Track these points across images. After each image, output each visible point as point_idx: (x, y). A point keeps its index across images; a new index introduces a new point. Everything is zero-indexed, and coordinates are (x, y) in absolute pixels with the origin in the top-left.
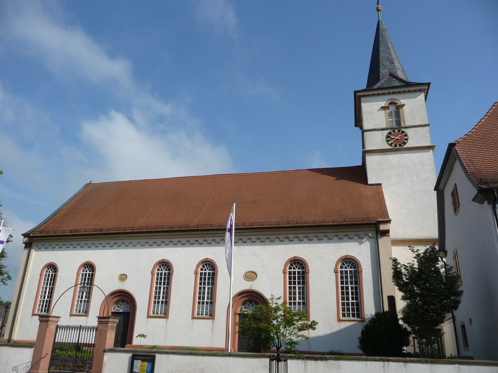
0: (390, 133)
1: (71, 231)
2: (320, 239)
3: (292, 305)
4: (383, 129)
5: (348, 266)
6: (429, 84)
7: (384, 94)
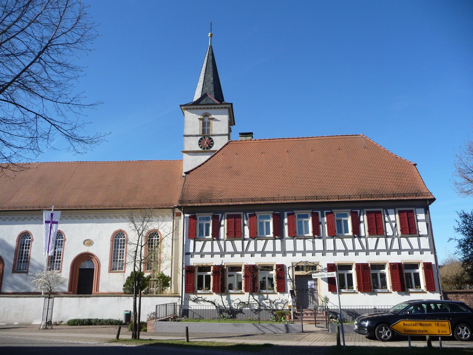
0: (201, 139)
4: (197, 136)
5: (120, 236)
7: (200, 108)
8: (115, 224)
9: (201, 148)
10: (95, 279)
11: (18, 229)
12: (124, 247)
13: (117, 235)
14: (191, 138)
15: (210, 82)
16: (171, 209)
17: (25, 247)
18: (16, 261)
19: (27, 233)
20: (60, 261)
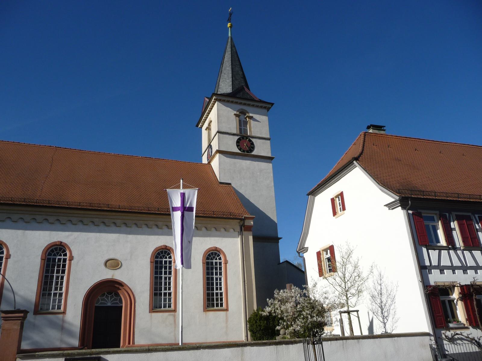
0: (239, 139)
2: (85, 224)
3: (157, 295)
4: (234, 135)
5: (214, 257)
6: (272, 104)
7: (236, 103)
8: (157, 236)
9: (240, 150)
13: (52, 251)
14: (227, 136)
16: (239, 221)
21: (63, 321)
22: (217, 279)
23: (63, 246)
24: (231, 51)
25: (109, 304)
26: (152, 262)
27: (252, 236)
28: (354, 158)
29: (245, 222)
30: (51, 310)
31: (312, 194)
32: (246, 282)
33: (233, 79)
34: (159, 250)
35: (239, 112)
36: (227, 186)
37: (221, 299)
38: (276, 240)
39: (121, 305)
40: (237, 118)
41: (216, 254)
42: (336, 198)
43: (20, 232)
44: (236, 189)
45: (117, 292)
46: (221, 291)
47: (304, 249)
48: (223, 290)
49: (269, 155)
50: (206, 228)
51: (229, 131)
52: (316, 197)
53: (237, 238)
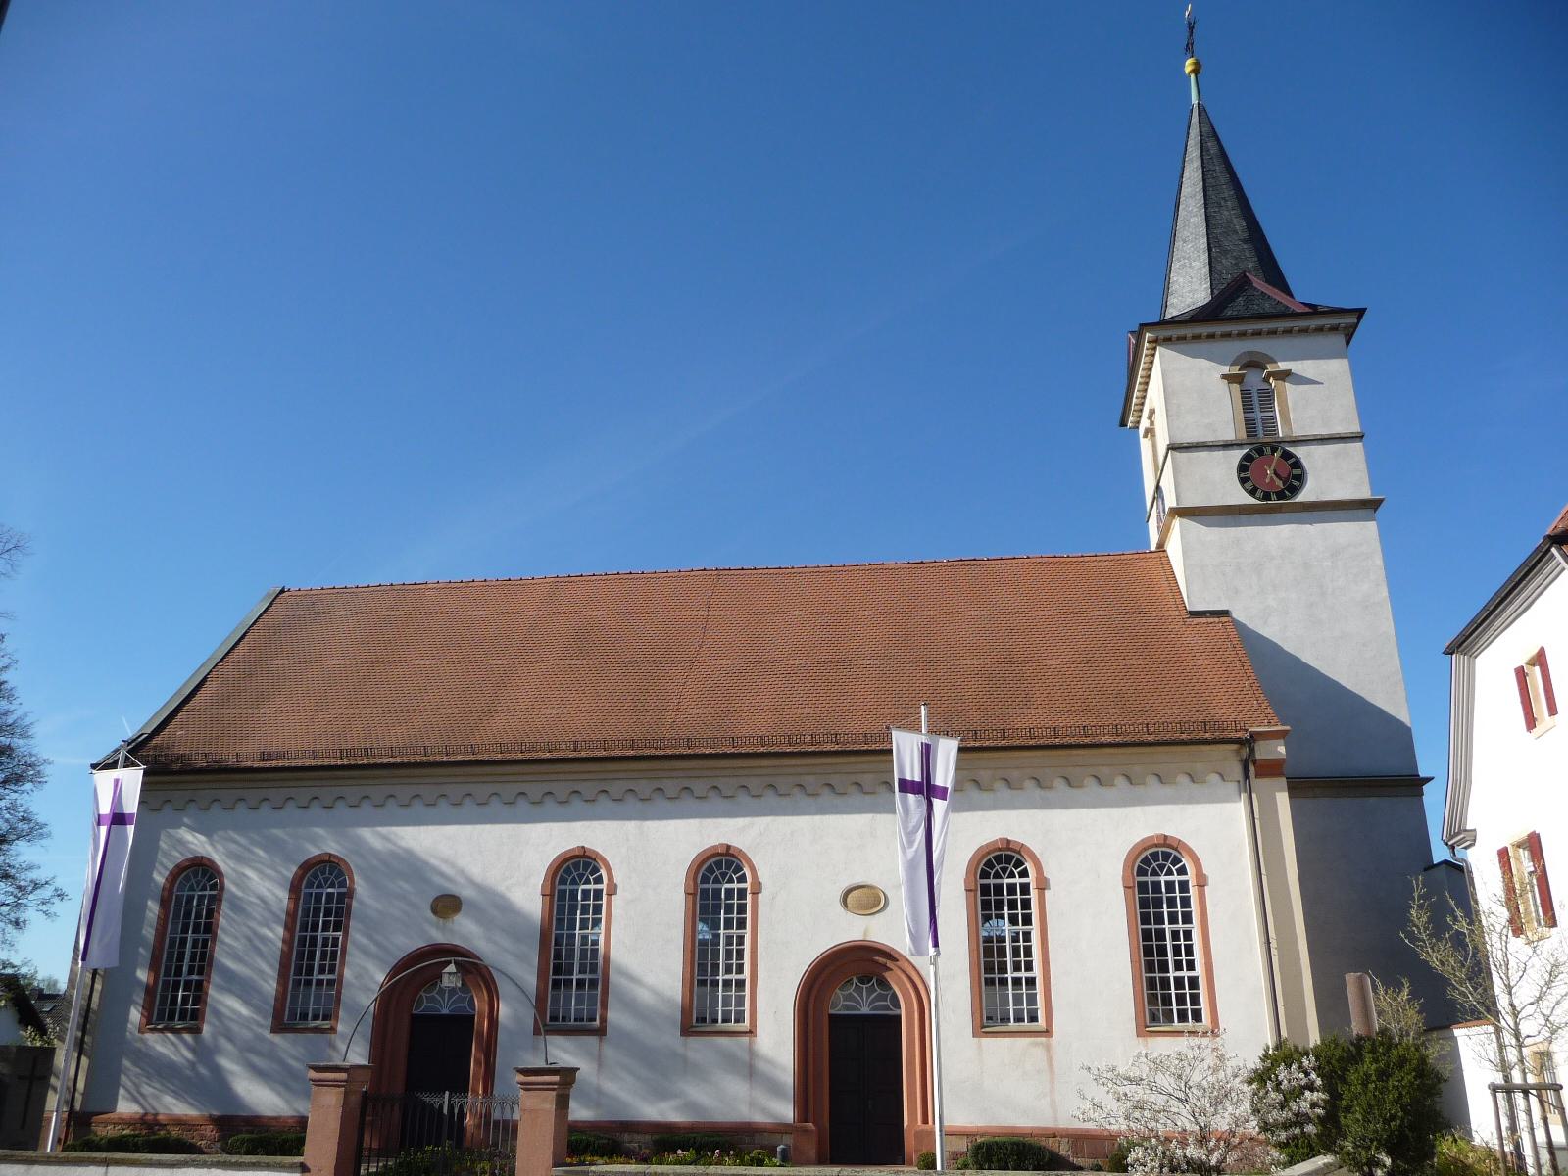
0: (1247, 457)
1: (263, 757)
3: (995, 984)
4: (1227, 446)
5: (1162, 867)
6: (1360, 312)
7: (1227, 336)
8: (980, 813)
9: (1252, 492)
10: (911, 1063)
11: (549, 840)
12: (742, 924)
13: (710, 870)
14: (1204, 454)
15: (1234, 236)
16: (1235, 746)
17: (324, 922)
18: (289, 978)
19: (584, 856)
20: (593, 983)
21: (751, 1052)
22: (1175, 935)
23: (733, 855)
24: (1202, 155)
25: (865, 1010)
26: (971, 890)
27: (1286, 794)
28: (1549, 536)
29: (1256, 748)
30: (720, 1025)
31: (1463, 647)
32: (1274, 944)
33: (1214, 254)
34: (988, 853)
35: (1238, 367)
36: (1217, 620)
37: (1195, 999)
38: (1414, 785)
39: (895, 1012)
40: (1236, 388)
41: (1166, 856)
42: (1534, 665)
43: (631, 826)
44: (1249, 626)
45: (884, 977)
46: (1192, 974)
47: (1462, 836)
48: (1199, 971)
49: (1365, 493)
50: (1128, 778)
51: (1209, 438)
52: (1476, 657)
53: (1235, 801)
